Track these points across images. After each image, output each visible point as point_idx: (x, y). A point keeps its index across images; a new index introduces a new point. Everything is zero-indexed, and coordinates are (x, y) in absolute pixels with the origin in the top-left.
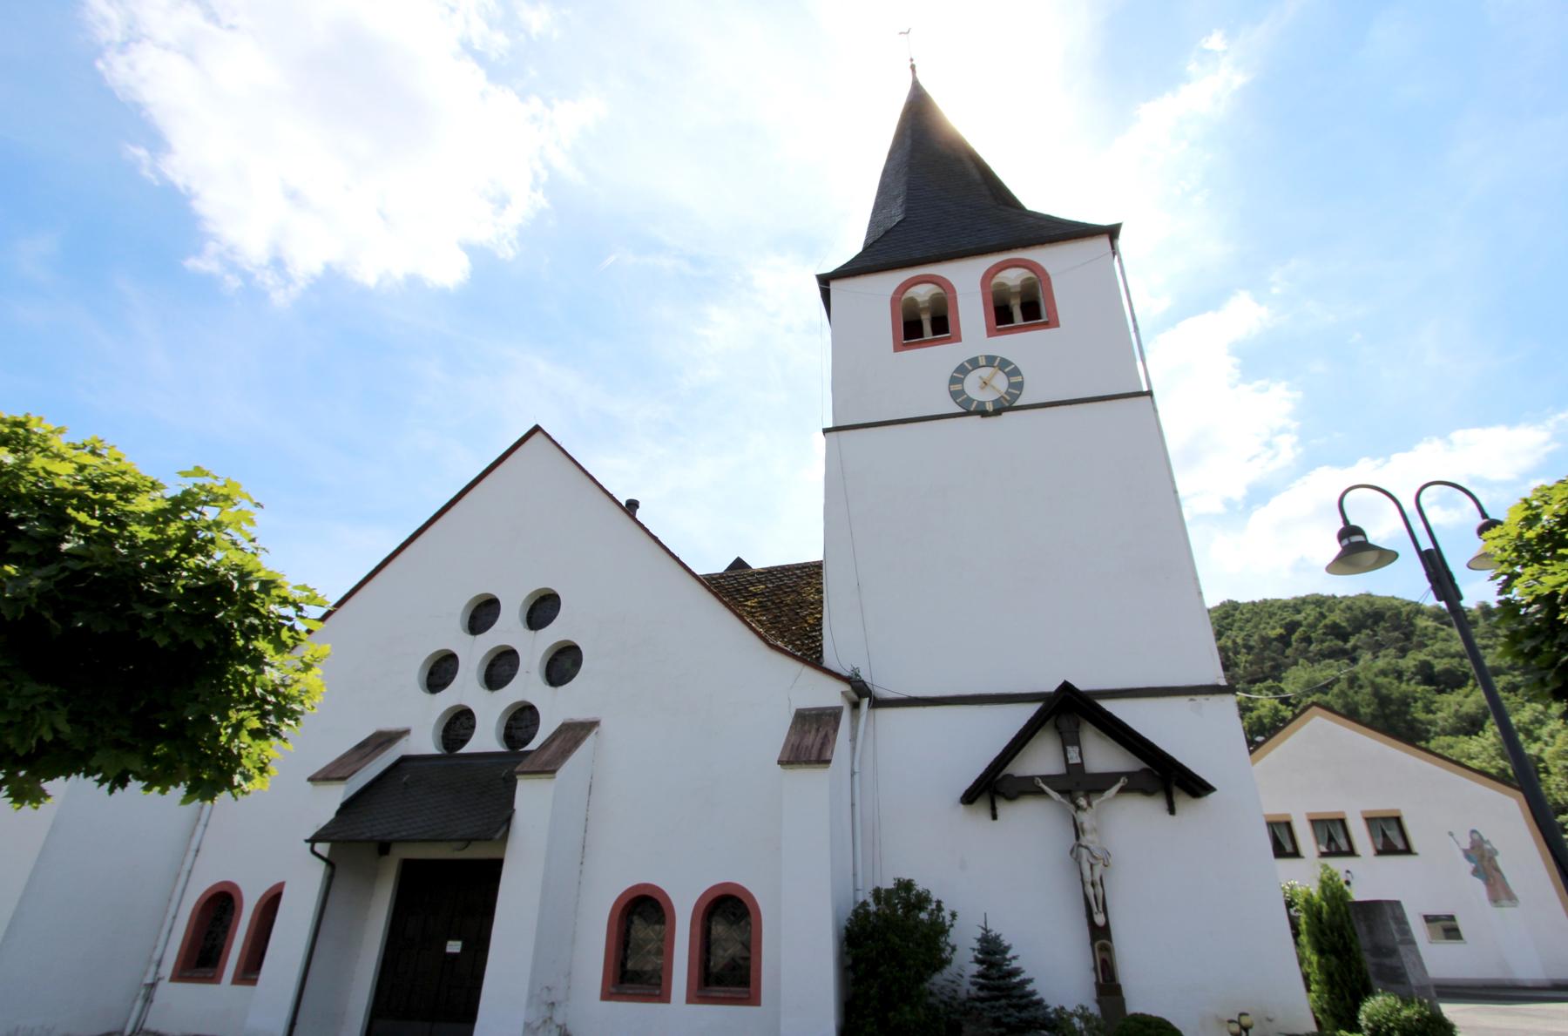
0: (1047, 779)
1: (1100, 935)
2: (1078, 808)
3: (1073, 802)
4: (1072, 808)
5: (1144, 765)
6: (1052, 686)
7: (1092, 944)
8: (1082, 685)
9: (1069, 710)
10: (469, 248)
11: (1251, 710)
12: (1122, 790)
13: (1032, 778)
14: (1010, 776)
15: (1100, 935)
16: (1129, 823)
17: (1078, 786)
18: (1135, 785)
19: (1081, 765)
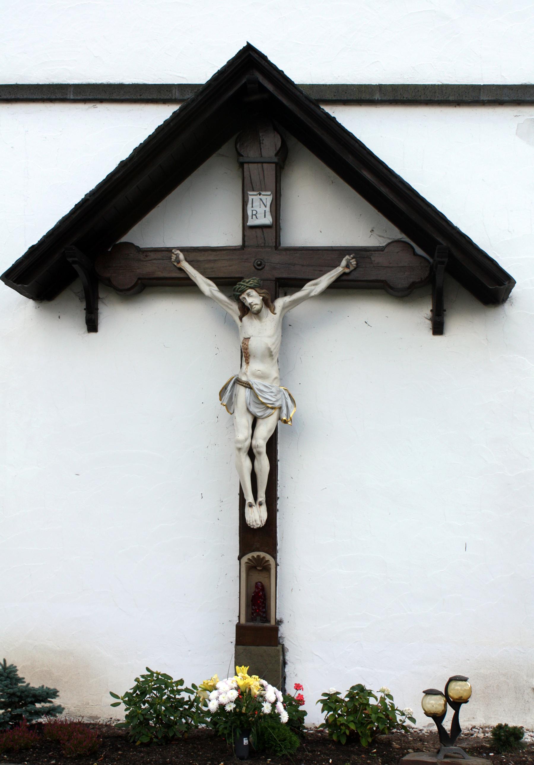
0: (194, 254)
1: (259, 543)
2: (245, 310)
3: (236, 298)
4: (234, 308)
5: (397, 234)
6: (200, 69)
7: (239, 559)
8: (302, 66)
9: (249, 115)
10: (248, 43)
11: (240, 701)
12: (342, 288)
13: (169, 250)
14: (130, 245)
15: (259, 543)
16: (363, 363)
17: (264, 271)
18: (360, 278)
19: (276, 227)
